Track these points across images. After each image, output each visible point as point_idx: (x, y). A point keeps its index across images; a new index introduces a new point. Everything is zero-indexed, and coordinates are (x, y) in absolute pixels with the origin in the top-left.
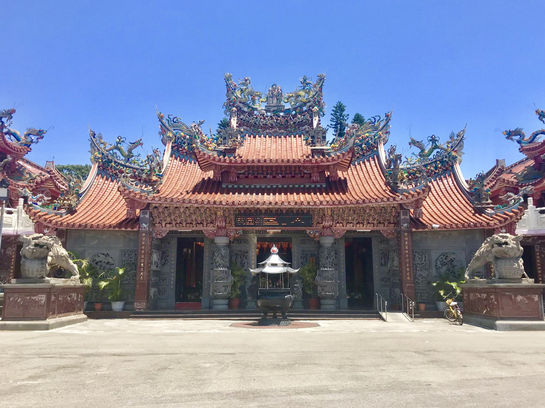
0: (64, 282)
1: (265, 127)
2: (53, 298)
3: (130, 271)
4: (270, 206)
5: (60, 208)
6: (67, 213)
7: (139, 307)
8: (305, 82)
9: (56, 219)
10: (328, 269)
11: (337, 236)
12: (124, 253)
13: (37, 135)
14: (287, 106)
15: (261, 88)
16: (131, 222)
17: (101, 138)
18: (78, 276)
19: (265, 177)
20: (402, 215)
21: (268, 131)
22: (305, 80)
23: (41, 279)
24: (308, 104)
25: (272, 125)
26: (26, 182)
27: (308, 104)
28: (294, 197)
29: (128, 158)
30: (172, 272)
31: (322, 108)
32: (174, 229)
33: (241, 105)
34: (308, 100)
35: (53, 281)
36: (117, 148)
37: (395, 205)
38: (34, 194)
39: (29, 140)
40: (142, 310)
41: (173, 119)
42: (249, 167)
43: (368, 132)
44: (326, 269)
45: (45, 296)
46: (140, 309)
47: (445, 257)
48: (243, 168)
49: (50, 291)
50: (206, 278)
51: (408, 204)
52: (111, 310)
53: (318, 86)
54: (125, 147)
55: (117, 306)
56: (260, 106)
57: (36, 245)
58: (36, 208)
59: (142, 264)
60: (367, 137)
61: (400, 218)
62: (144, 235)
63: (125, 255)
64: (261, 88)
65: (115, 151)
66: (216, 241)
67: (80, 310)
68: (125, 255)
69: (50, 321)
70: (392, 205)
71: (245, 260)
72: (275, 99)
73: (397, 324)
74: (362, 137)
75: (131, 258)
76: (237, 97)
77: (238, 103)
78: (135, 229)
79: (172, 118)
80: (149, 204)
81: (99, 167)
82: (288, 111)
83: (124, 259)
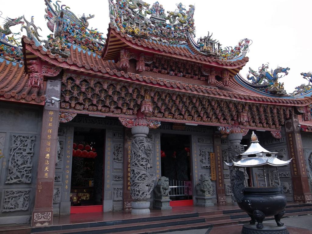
3: (22, 164)
7: (43, 220)
12: (14, 139)
19: (168, 73)
25: (157, 34)
30: (67, 169)
32: (84, 112)
34: (184, 21)
40: (46, 224)
41: (62, 6)
45: (43, 104)
46: (42, 223)
47: (136, 172)
50: (108, 176)
59: (48, 155)
61: (292, 120)
62: (51, 113)
63: (15, 141)
68: (15, 141)
75: (24, 146)
79: (60, 4)
83: (14, 146)
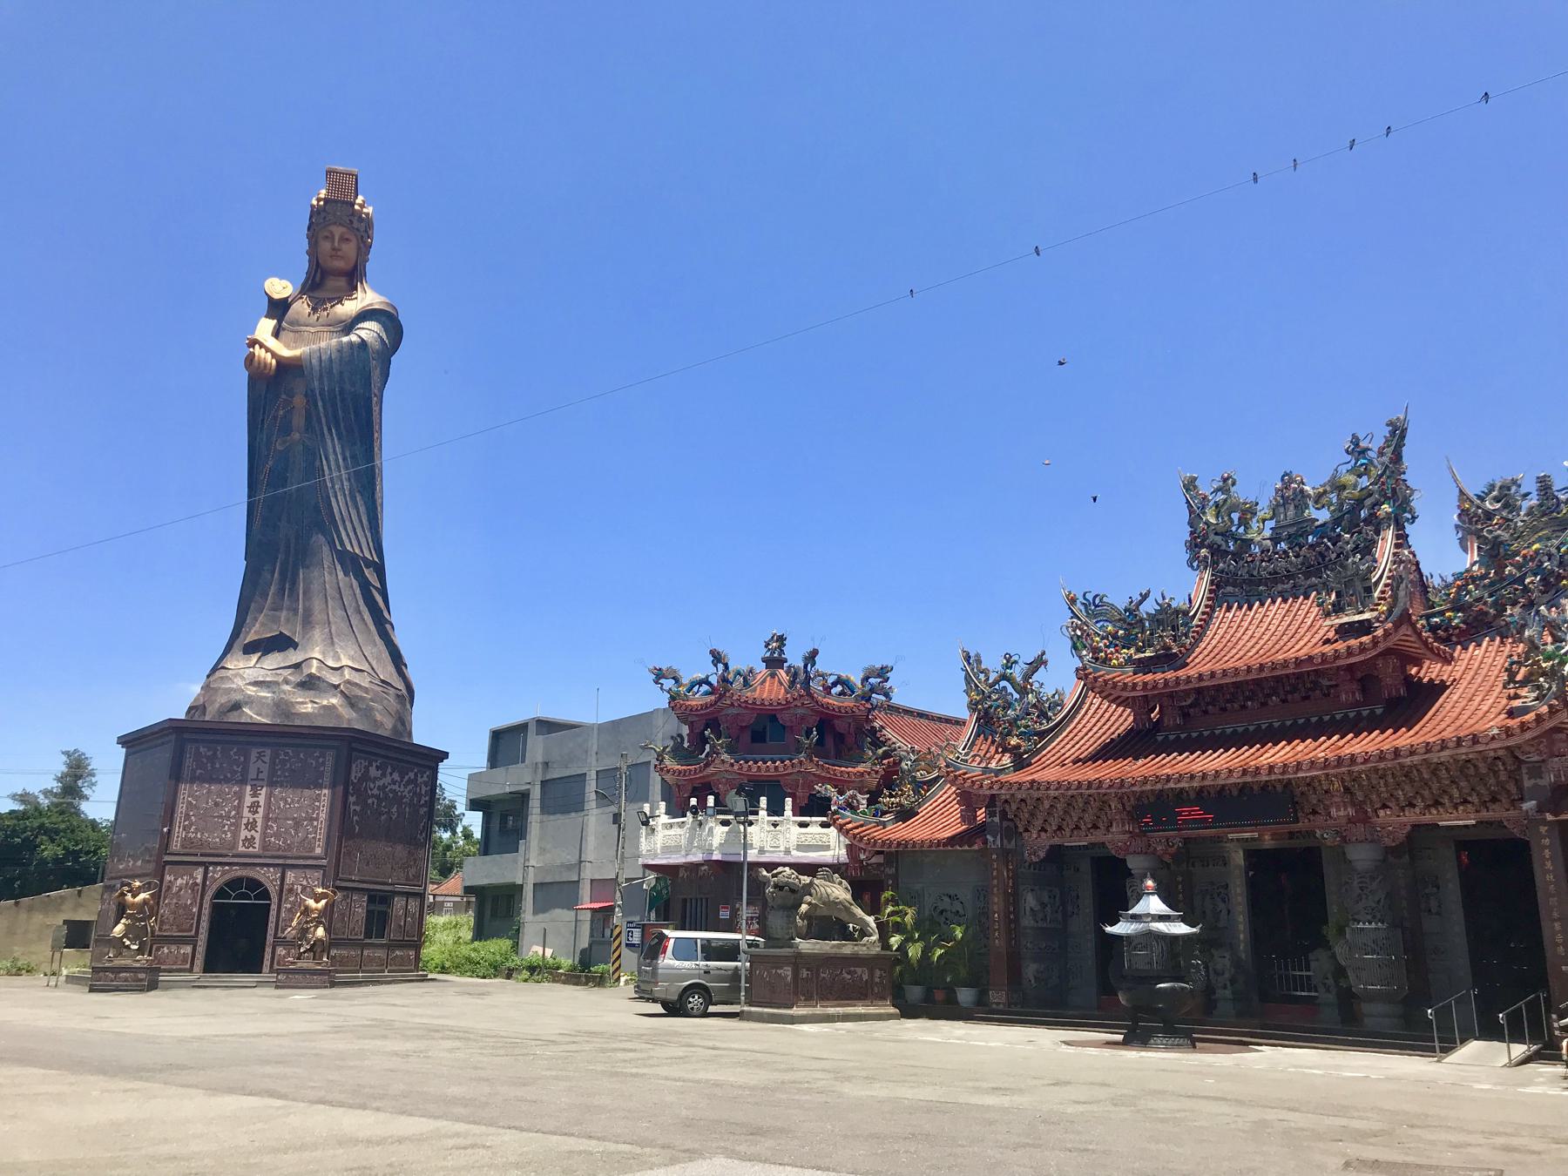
0: (838, 946)
1: (1275, 577)
2: (804, 973)
4: (1206, 783)
5: (884, 813)
6: (896, 820)
8: (1357, 450)
9: (879, 834)
10: (1367, 925)
11: (1388, 841)
13: (879, 676)
14: (1323, 516)
15: (1258, 490)
16: (974, 833)
17: (979, 662)
18: (875, 938)
20: (1525, 777)
21: (1280, 587)
22: (1357, 445)
23: (788, 942)
24: (1368, 502)
26: (869, 764)
27: (1368, 502)
28: (1278, 754)
29: (1023, 691)
31: (1407, 501)
33: (1218, 539)
35: (806, 946)
36: (1004, 677)
37: (1501, 753)
38: (841, 793)
39: (867, 688)
42: (1199, 691)
43: (1539, 540)
44: (1361, 925)
48: (1187, 693)
49: (799, 960)
51: (1527, 749)
52: (957, 1003)
53: (1389, 451)
54: (1017, 673)
55: (965, 996)
56: (1260, 532)
57: (776, 886)
58: (843, 817)
60: (1537, 552)
64: (1258, 490)
65: (1003, 683)
66: (1349, 857)
67: (884, 999)
69: (795, 1011)
70: (1492, 754)
71: (1222, 906)
72: (1292, 507)
73: (1482, 1067)
74: (1525, 557)
76: (1208, 523)
77: (1212, 537)
78: (976, 847)
80: (993, 796)
81: (978, 720)
82: (1322, 530)
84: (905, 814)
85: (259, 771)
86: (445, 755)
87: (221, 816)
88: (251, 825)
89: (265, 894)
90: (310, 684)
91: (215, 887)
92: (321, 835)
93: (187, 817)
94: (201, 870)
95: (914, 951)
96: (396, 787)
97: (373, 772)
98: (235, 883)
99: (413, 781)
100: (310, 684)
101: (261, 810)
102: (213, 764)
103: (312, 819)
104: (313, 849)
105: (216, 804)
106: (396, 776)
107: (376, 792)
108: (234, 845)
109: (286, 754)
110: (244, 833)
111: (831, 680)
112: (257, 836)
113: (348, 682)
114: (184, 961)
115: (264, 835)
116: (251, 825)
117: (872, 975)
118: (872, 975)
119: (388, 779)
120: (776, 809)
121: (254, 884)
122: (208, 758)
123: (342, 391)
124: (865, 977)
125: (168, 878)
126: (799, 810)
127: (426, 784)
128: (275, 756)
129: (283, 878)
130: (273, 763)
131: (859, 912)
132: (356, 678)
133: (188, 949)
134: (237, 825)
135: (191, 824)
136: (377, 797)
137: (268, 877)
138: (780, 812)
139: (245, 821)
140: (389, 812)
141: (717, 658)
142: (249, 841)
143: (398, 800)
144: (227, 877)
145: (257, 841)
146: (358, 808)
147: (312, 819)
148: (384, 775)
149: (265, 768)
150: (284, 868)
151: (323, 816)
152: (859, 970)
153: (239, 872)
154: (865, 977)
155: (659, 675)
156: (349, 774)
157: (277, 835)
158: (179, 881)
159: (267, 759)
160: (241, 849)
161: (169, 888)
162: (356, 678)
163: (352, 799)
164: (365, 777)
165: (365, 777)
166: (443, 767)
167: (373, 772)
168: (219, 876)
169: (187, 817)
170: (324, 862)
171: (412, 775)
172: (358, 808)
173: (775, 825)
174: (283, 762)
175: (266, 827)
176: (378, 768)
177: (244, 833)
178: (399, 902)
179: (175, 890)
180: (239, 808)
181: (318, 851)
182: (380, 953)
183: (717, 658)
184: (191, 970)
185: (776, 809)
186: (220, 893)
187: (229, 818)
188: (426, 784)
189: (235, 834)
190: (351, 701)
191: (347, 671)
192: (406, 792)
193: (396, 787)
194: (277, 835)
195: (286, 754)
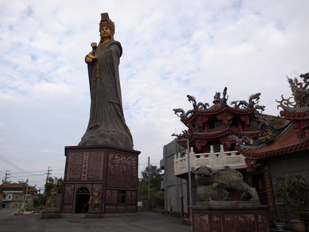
0: (236, 204)
57: (198, 174)
84: (270, 143)
85: (86, 159)
86: (139, 153)
87: (77, 171)
88: (85, 173)
89: (89, 192)
90: (102, 136)
91: (77, 190)
92: (101, 175)
93: (70, 171)
94: (73, 185)
95: (73, 176)
96: (125, 161)
97: (116, 157)
98: (81, 189)
99: (131, 160)
100: (102, 136)
101: (87, 169)
102: (75, 157)
103: (99, 170)
104: (100, 179)
105: (76, 168)
106: (124, 158)
107: (118, 162)
108: (81, 179)
109: (92, 153)
110: (83, 175)
111: (238, 104)
112: (86, 175)
113: (111, 134)
114: (70, 210)
115: (88, 175)
116: (85, 173)
117: (256, 218)
118: (256, 218)
119: (122, 159)
120: (217, 150)
121: (86, 189)
122: (74, 156)
123: (107, 63)
124: (253, 219)
125: (66, 188)
126: (226, 149)
127: (135, 160)
128: (90, 154)
129: (93, 187)
130: (89, 156)
131: (246, 186)
132: (113, 133)
133: (71, 207)
134: (81, 173)
135: (71, 173)
136: (119, 164)
137: (89, 187)
138: (218, 150)
139: (83, 172)
140: (123, 168)
141: (190, 98)
142: (84, 177)
143: (126, 165)
144: (79, 187)
145: (86, 177)
146: (112, 167)
147: (99, 170)
148: (120, 158)
149: (87, 157)
150: (93, 184)
151: (102, 169)
152: (249, 216)
153: (82, 186)
154: (253, 219)
155: (176, 111)
156: (108, 157)
157: (91, 175)
158: (69, 188)
159: (88, 155)
160: (82, 179)
161: (66, 190)
162: (113, 133)
163: (110, 164)
164: (114, 158)
165: (114, 158)
166: (139, 156)
167: (116, 157)
168: (78, 187)
169: (70, 171)
170: (103, 182)
171: (130, 158)
172: (112, 167)
173: (217, 155)
174: (92, 156)
175: (88, 173)
176: (118, 156)
177: (83, 175)
178: (129, 193)
179: (68, 191)
180: (81, 169)
181: (101, 179)
182: (123, 207)
183: (190, 98)
184: (72, 212)
185: (217, 150)
186: (78, 192)
187: (79, 171)
188: (135, 160)
189: (81, 176)
190: (112, 139)
191: (111, 131)
192: (128, 163)
193: (125, 161)
194: (91, 175)
195: (92, 153)
